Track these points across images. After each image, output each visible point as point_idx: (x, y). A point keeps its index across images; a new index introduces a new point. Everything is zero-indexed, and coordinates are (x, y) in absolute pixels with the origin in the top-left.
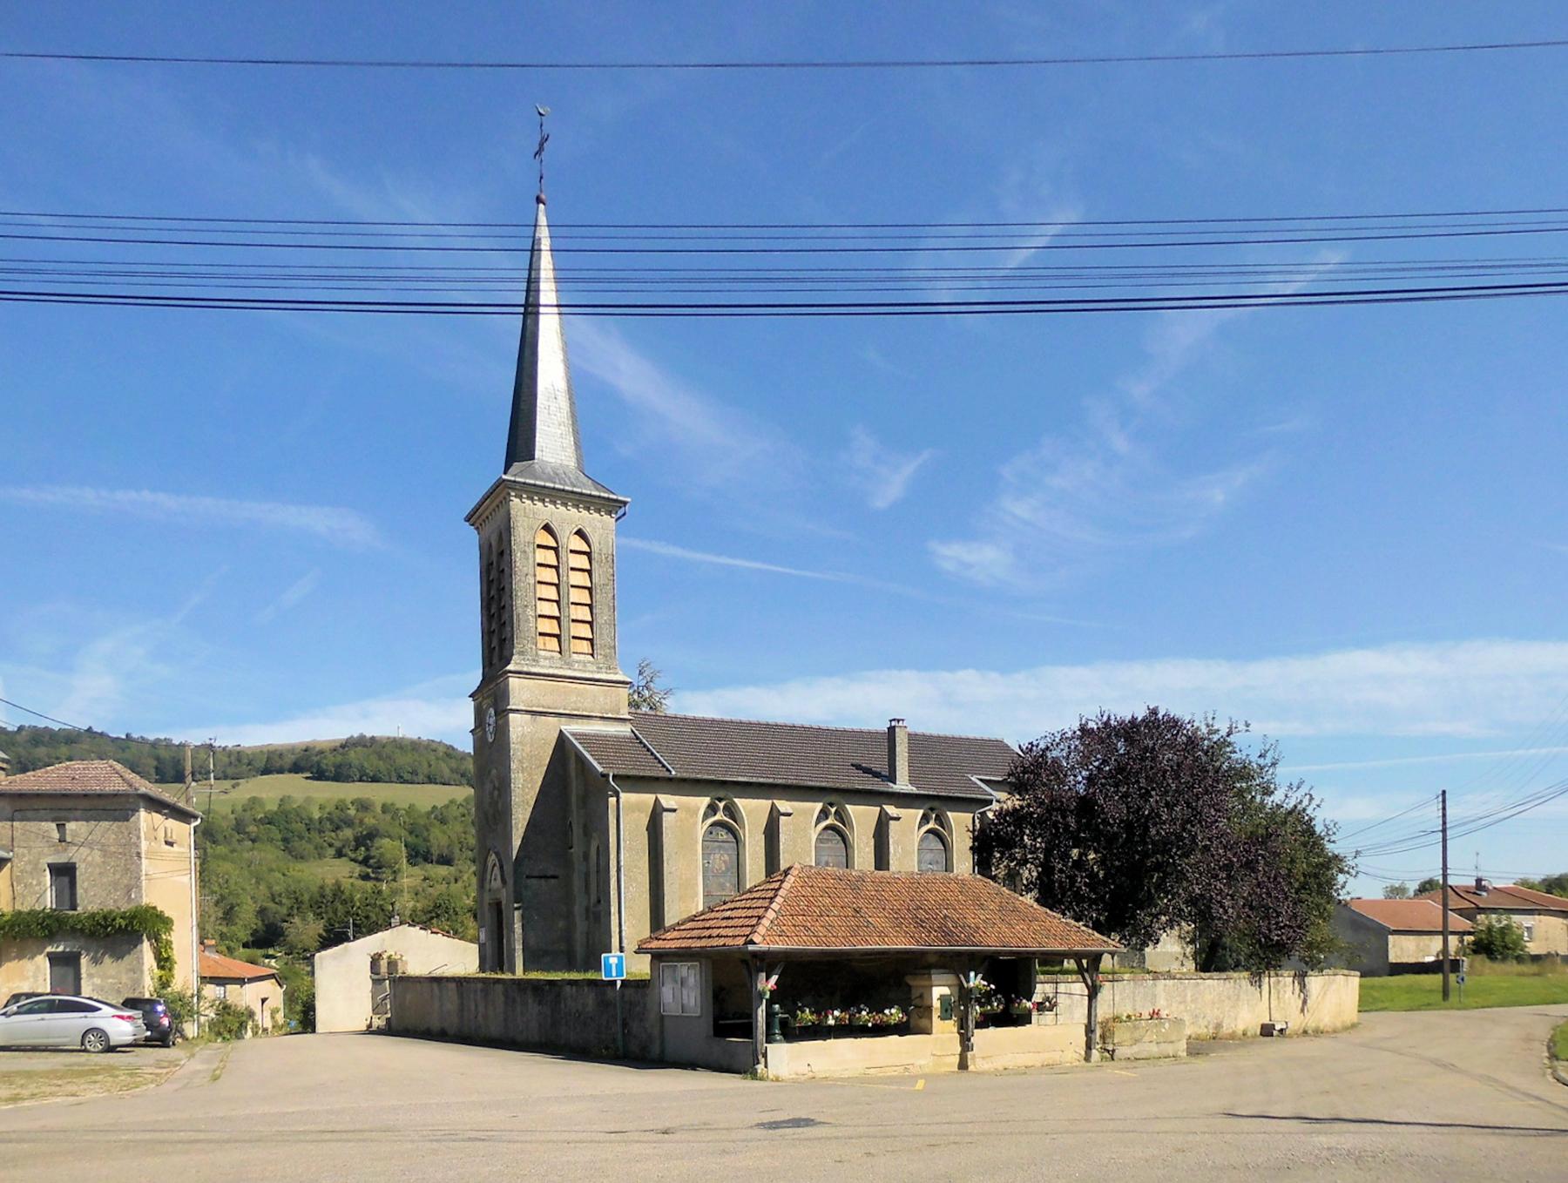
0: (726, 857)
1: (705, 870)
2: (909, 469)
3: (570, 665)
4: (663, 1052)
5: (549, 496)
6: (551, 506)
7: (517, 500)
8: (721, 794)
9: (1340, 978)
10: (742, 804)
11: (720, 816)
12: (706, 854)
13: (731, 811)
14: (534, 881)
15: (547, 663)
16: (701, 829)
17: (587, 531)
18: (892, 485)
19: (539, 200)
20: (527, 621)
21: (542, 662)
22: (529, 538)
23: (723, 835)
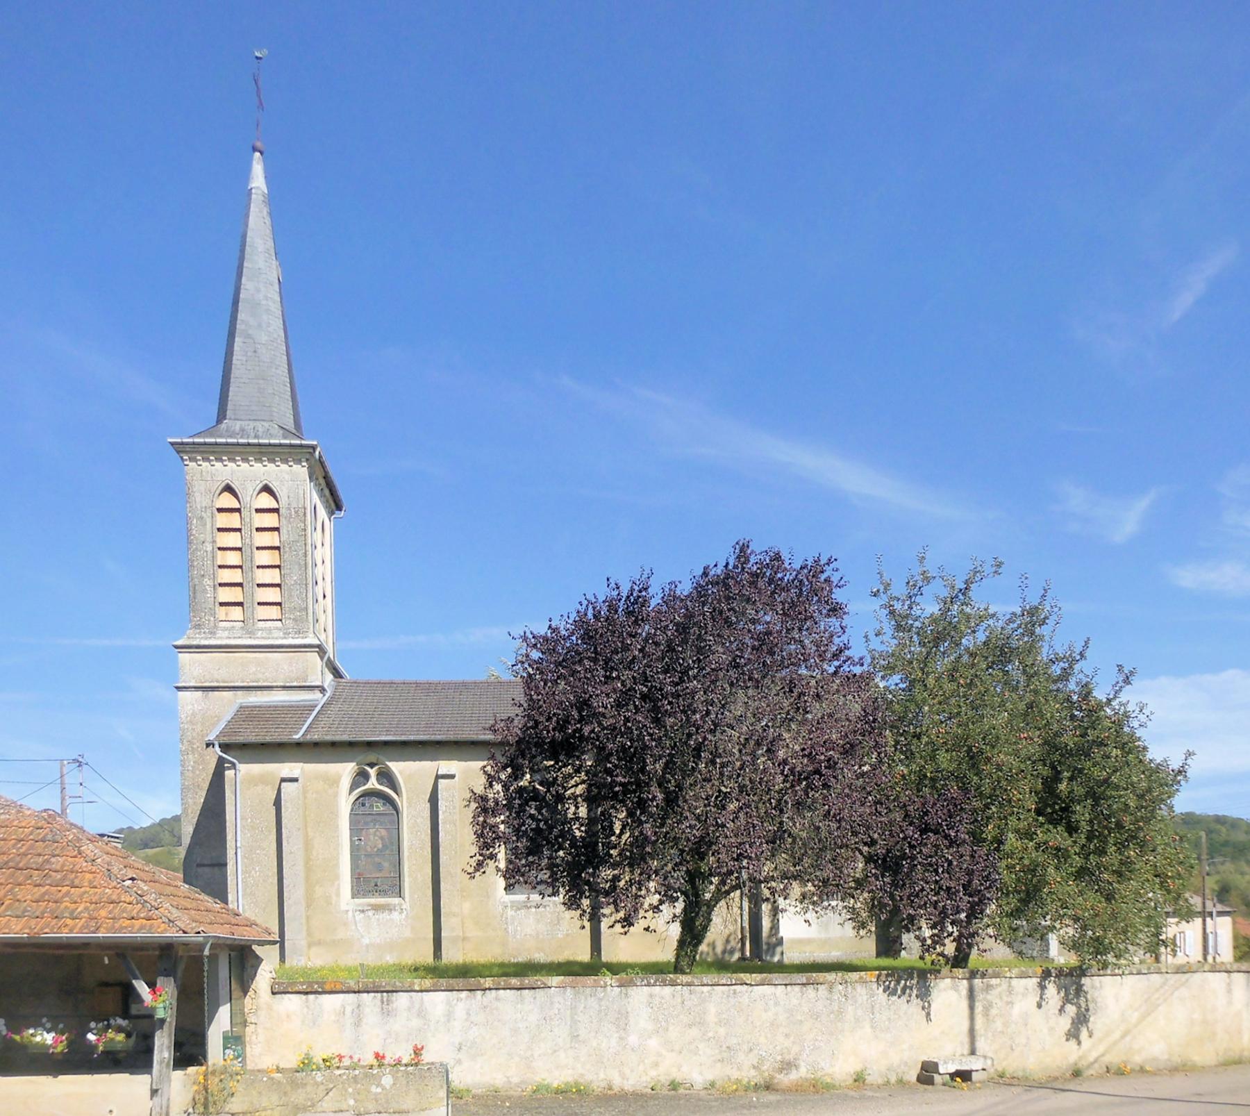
0: (384, 833)
1: (355, 850)
2: (1142, 504)
3: (251, 634)
4: (1042, 987)
5: (239, 453)
6: (231, 465)
7: (193, 464)
8: (372, 757)
9: (515, 1080)
10: (397, 768)
11: (373, 783)
12: (355, 829)
13: (387, 777)
14: (207, 870)
15: (226, 634)
16: (345, 803)
17: (274, 486)
18: (1127, 520)
19: (255, 149)
20: (205, 591)
21: (220, 633)
22: (206, 502)
23: (379, 807)
